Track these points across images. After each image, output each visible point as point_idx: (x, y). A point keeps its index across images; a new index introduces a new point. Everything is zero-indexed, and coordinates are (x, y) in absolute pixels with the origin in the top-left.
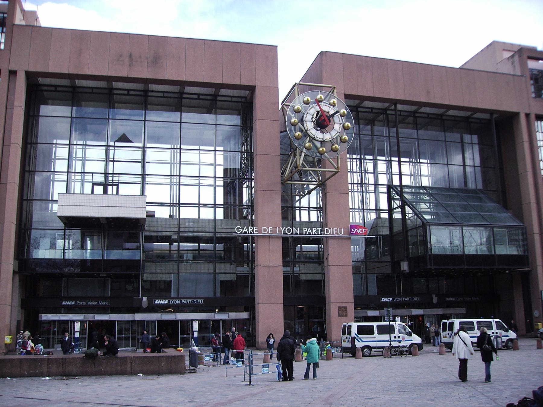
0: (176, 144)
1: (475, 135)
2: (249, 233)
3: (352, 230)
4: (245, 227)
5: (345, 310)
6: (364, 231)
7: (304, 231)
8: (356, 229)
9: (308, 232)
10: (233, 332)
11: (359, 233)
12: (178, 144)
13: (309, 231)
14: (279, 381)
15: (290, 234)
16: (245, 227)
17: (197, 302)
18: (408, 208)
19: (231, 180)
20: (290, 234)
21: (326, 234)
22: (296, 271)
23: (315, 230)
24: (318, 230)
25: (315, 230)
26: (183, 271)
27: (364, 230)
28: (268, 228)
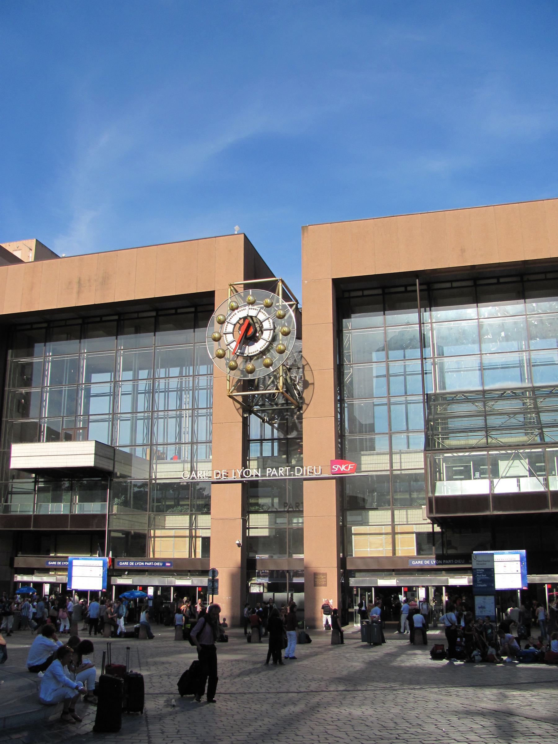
0: (188, 366)
2: (278, 476)
3: (333, 467)
5: (324, 578)
6: (350, 467)
7: (268, 472)
8: (338, 466)
9: (273, 473)
11: (342, 470)
12: (113, 372)
13: (274, 472)
14: (308, 364)
16: (274, 469)
17: (158, 564)
18: (133, 445)
19: (66, 418)
21: (296, 474)
22: (350, 522)
25: (281, 470)
26: (405, 520)
27: (351, 466)
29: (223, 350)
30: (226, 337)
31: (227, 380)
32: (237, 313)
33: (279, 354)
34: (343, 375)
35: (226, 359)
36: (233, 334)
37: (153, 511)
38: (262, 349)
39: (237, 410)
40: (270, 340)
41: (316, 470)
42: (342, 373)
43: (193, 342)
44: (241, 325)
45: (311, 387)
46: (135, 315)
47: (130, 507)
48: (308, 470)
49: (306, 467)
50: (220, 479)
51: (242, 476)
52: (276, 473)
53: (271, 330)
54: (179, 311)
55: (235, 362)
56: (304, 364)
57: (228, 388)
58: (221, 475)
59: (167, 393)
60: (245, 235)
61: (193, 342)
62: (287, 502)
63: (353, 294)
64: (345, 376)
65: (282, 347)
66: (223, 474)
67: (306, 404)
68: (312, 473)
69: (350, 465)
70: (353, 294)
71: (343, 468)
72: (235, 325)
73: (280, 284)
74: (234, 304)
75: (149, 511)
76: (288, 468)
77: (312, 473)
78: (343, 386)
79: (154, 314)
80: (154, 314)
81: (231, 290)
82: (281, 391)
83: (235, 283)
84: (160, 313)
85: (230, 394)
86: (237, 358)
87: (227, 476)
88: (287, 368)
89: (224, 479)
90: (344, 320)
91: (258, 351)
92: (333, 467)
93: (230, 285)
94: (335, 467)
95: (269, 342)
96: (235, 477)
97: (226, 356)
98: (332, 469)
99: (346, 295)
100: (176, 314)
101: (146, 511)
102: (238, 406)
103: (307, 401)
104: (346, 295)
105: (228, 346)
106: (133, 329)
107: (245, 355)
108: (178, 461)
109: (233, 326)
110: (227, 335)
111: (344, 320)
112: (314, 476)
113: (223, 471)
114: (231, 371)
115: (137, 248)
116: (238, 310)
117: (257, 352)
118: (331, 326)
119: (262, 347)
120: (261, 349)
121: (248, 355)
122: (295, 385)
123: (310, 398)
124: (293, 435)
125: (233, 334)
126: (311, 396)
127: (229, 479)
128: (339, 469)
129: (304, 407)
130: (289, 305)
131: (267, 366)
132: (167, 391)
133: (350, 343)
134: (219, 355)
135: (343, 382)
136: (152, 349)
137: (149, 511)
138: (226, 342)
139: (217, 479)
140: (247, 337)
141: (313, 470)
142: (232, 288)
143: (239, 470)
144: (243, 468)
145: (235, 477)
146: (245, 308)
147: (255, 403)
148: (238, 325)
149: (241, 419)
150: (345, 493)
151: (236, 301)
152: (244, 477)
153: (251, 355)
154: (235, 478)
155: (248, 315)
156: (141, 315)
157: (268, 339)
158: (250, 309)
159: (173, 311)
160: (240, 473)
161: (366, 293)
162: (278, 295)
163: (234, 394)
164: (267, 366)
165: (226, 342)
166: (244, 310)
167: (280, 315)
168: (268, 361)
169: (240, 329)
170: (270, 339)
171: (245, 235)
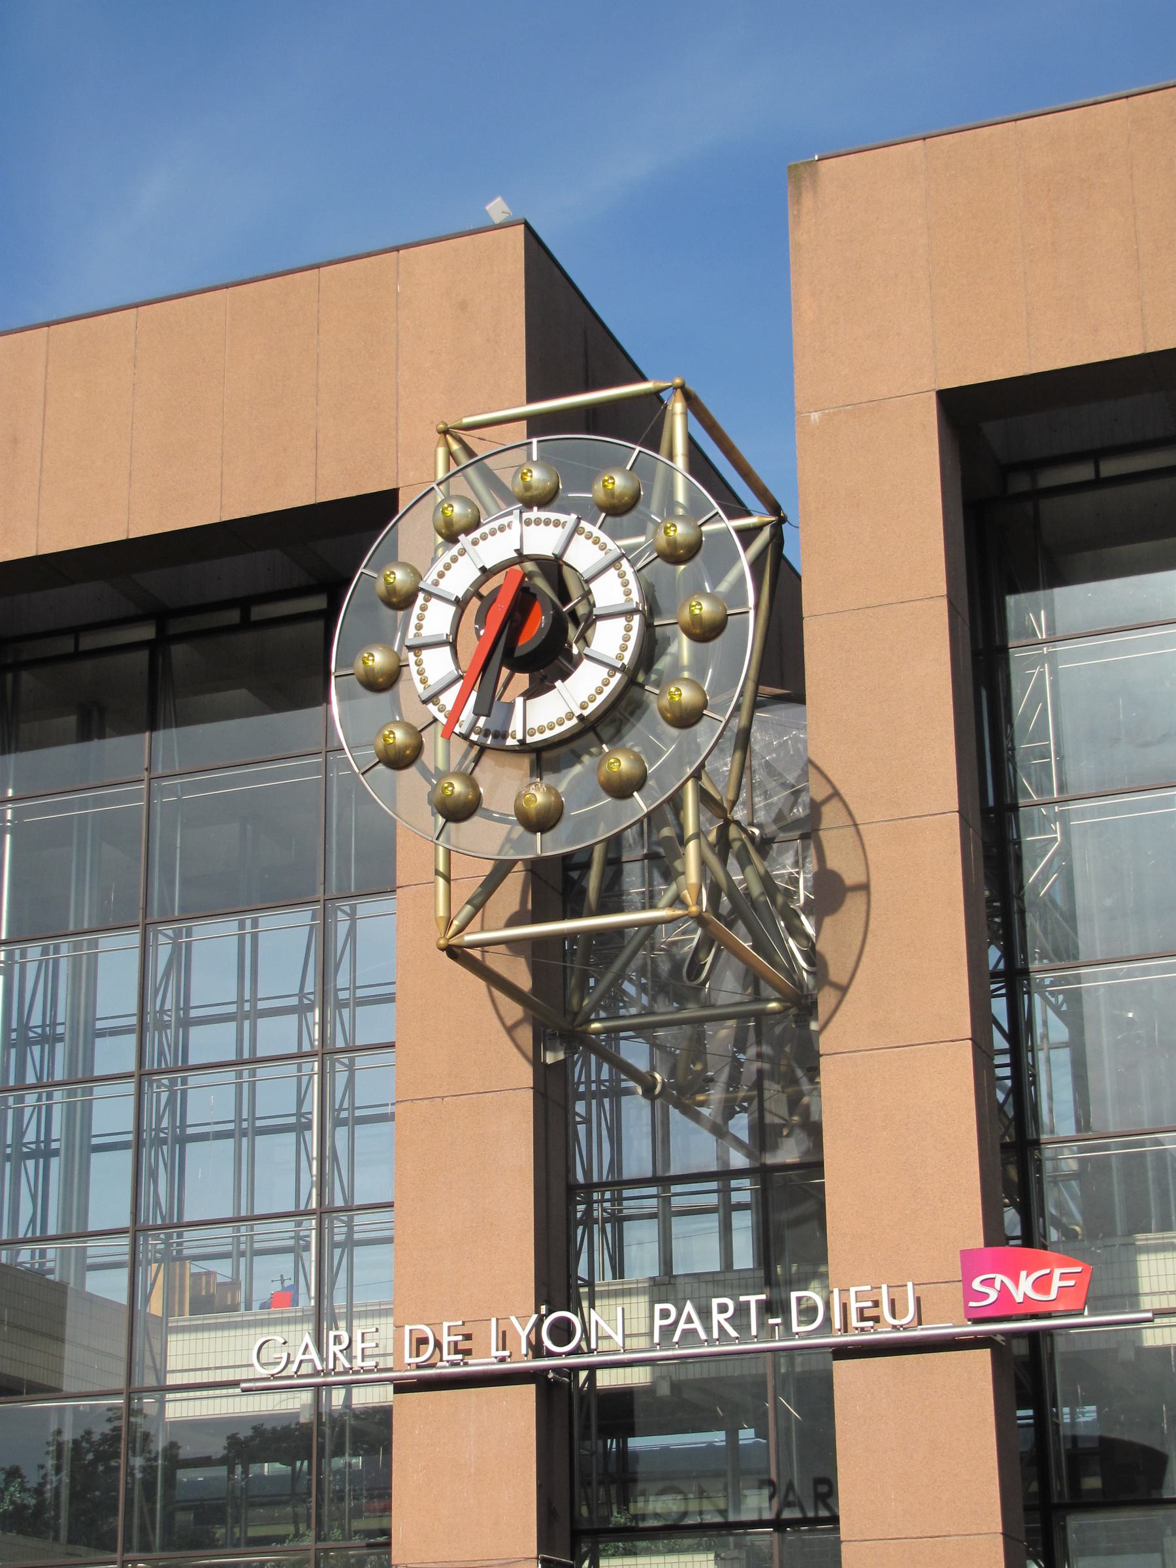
1: (1011, 1059)
2: (710, 1341)
3: (976, 1285)
4: (689, 1308)
6: (1056, 1283)
8: (999, 1278)
9: (682, 1326)
10: (764, 845)
14: (836, 794)
15: (568, 1354)
16: (689, 1308)
20: (568, 1354)
23: (723, 1309)
24: (742, 1310)
25: (723, 1309)
27: (1063, 1276)
28: (435, 1325)
29: (410, 728)
30: (419, 663)
31: (437, 872)
32: (469, 547)
33: (674, 732)
34: (1019, 859)
35: (425, 773)
36: (453, 645)
37: (146, 1547)
38: (592, 707)
39: (510, 1030)
40: (626, 661)
41: (892, 1303)
42: (1012, 849)
43: (322, 748)
44: (487, 602)
45: (853, 904)
46: (66, 645)
47: (56, 1538)
48: (854, 1306)
49: (844, 1291)
50: (433, 1366)
51: (537, 1350)
52: (697, 1324)
53: (628, 614)
54: (259, 612)
55: (470, 781)
56: (819, 797)
57: (442, 912)
58: (438, 1345)
59: (247, 1024)
60: (528, 228)
61: (322, 748)
62: (774, 1476)
63: (1051, 478)
64: (1026, 864)
65: (686, 695)
66: (445, 1340)
67: (835, 986)
68: (876, 1319)
69: (1057, 1272)
70: (1051, 478)
71: (1024, 1288)
72: (461, 604)
73: (678, 407)
74: (457, 511)
75: (127, 1548)
76: (753, 1299)
77: (876, 1319)
78: (1022, 912)
79: (147, 632)
80: (147, 632)
81: (450, 454)
82: (694, 909)
83: (467, 420)
84: (176, 627)
85: (454, 941)
86: (477, 760)
87: (467, 1352)
88: (752, 837)
89: (454, 1364)
90: (1011, 600)
91: (570, 715)
92: (976, 1285)
93: (445, 432)
94: (983, 1282)
95: (623, 669)
96: (506, 1353)
97: (426, 757)
98: (971, 1294)
99: (1020, 483)
100: (246, 624)
101: (114, 1550)
102: (514, 1011)
103: (837, 973)
104: (1020, 483)
105: (430, 706)
106: (71, 721)
107: (510, 742)
108: (290, 1312)
109: (452, 609)
110: (426, 654)
111: (1011, 600)
112: (883, 1334)
113: (446, 1325)
114: (452, 826)
115: (48, 325)
116: (476, 534)
117: (569, 724)
118: (941, 607)
119: (592, 700)
120: (583, 707)
121: (522, 742)
122: (791, 919)
123: (854, 958)
124: (789, 1153)
125: (453, 645)
126: (856, 951)
127: (477, 1364)
128: (1004, 1291)
129: (826, 999)
130: (739, 531)
131: (622, 789)
132: (246, 1016)
133: (1044, 710)
134: (391, 752)
135: (1021, 887)
136: (135, 796)
137: (127, 1548)
138: (420, 688)
139: (419, 1367)
140: (518, 653)
141: (876, 1304)
142: (455, 446)
143: (523, 1319)
144: (543, 1309)
145: (506, 1353)
146: (505, 521)
147: (596, 995)
148: (475, 603)
149: (525, 1074)
150: (1057, 1425)
151: (471, 495)
152: (551, 1354)
153: (538, 737)
154: (502, 1360)
155: (519, 552)
156: (89, 642)
157: (620, 657)
158: (528, 523)
159: (233, 616)
160: (523, 1332)
161: (1110, 468)
162: (671, 457)
163: (469, 938)
164: (622, 789)
165: (420, 688)
166: (502, 529)
167: (673, 544)
168: (621, 764)
169: (481, 619)
170: (627, 657)
171: (528, 228)
